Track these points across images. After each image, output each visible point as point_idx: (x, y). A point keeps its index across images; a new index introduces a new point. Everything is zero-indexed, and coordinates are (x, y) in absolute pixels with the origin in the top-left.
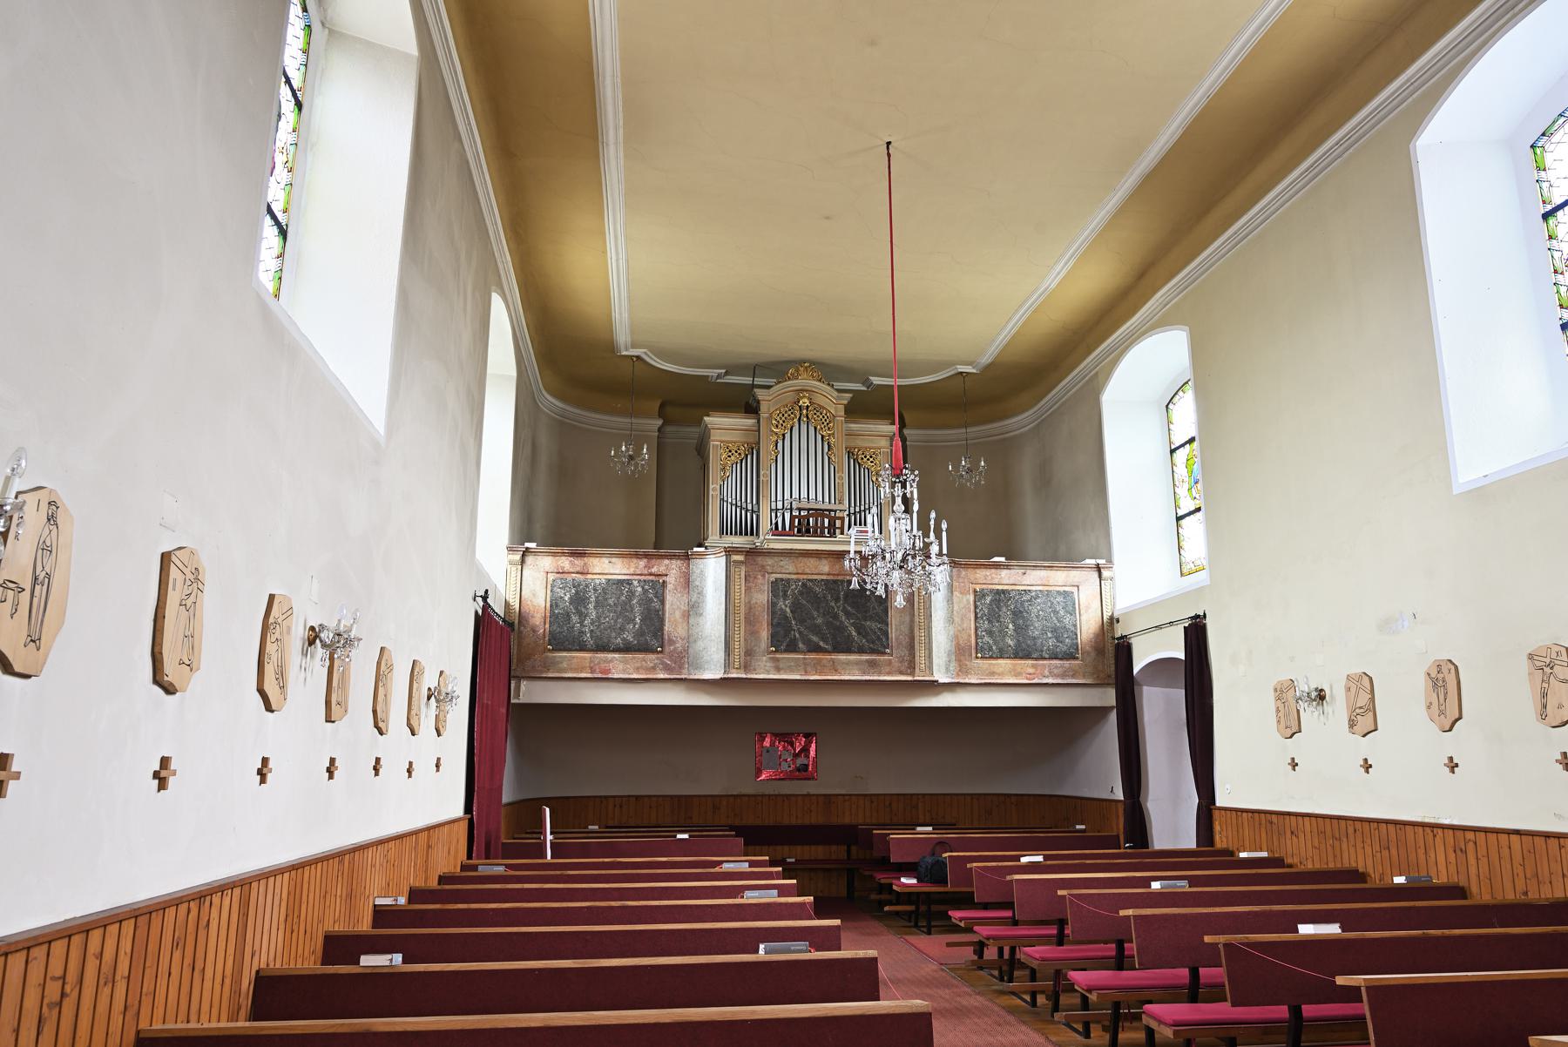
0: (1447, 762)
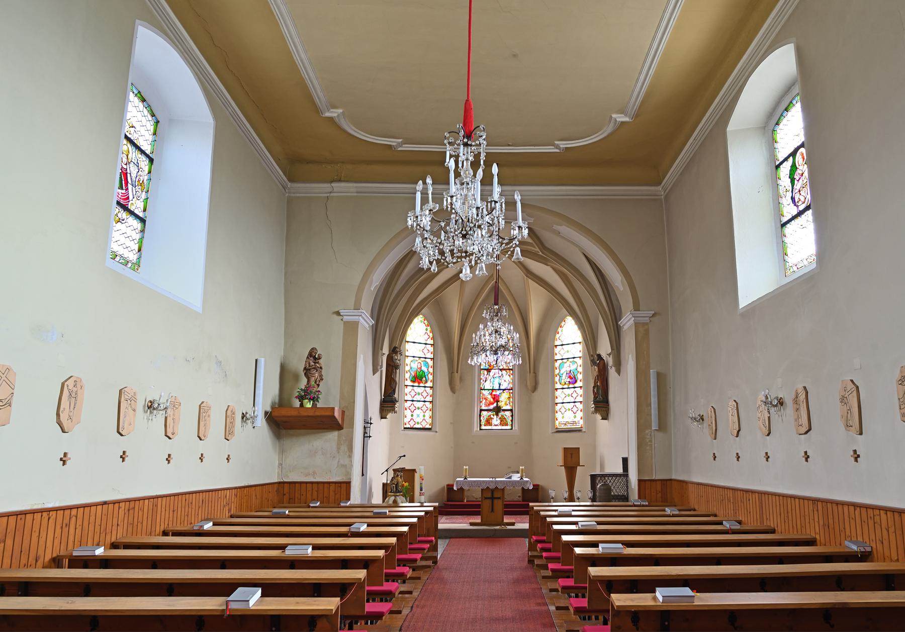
0: (852, 453)
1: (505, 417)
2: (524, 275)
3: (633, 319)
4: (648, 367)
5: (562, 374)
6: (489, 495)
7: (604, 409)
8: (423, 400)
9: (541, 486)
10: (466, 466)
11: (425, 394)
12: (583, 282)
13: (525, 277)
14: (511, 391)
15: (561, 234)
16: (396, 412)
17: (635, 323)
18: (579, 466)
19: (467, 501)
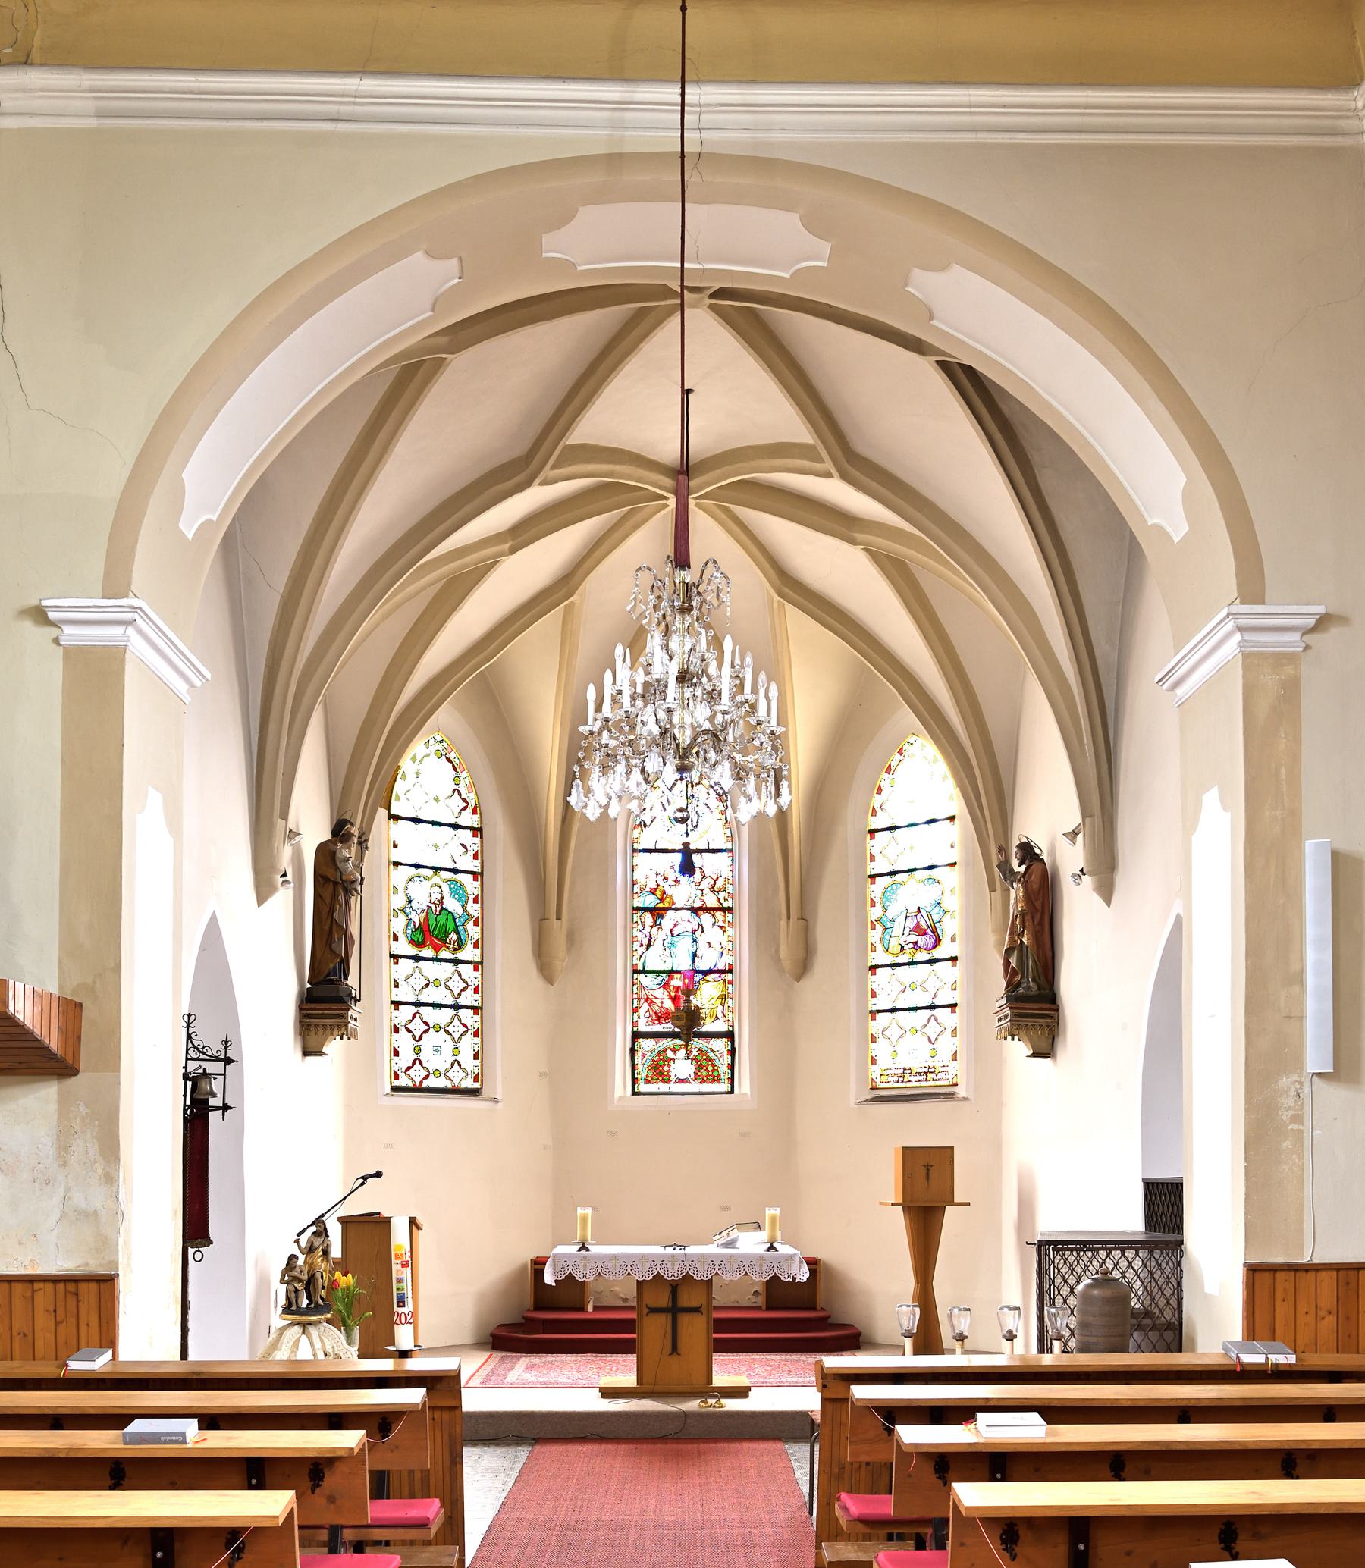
1: (711, 1054)
2: (772, 592)
3: (1238, 637)
4: (1292, 830)
5: (893, 921)
6: (664, 1301)
7: (1042, 1021)
8: (450, 1001)
9: (824, 1263)
10: (584, 1206)
11: (457, 985)
12: (987, 579)
13: (776, 597)
14: (729, 976)
15: (935, 322)
16: (353, 1035)
17: (1246, 656)
18: (952, 1203)
19: (596, 1308)
